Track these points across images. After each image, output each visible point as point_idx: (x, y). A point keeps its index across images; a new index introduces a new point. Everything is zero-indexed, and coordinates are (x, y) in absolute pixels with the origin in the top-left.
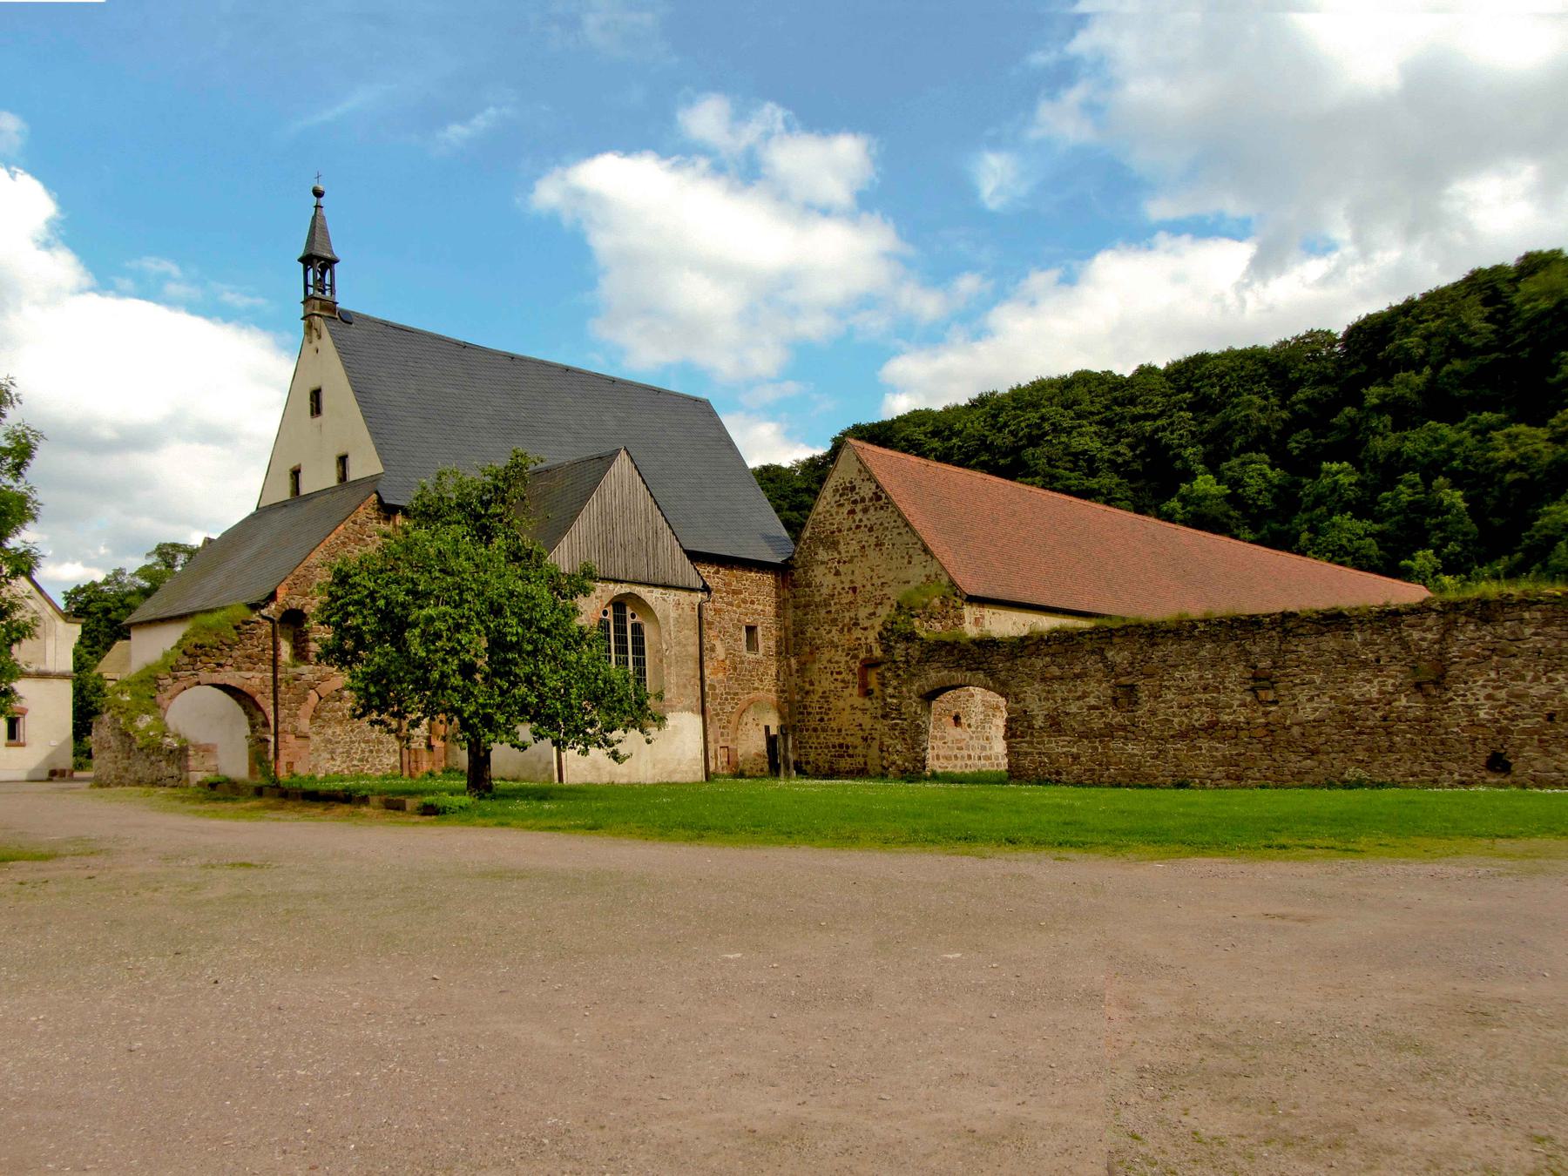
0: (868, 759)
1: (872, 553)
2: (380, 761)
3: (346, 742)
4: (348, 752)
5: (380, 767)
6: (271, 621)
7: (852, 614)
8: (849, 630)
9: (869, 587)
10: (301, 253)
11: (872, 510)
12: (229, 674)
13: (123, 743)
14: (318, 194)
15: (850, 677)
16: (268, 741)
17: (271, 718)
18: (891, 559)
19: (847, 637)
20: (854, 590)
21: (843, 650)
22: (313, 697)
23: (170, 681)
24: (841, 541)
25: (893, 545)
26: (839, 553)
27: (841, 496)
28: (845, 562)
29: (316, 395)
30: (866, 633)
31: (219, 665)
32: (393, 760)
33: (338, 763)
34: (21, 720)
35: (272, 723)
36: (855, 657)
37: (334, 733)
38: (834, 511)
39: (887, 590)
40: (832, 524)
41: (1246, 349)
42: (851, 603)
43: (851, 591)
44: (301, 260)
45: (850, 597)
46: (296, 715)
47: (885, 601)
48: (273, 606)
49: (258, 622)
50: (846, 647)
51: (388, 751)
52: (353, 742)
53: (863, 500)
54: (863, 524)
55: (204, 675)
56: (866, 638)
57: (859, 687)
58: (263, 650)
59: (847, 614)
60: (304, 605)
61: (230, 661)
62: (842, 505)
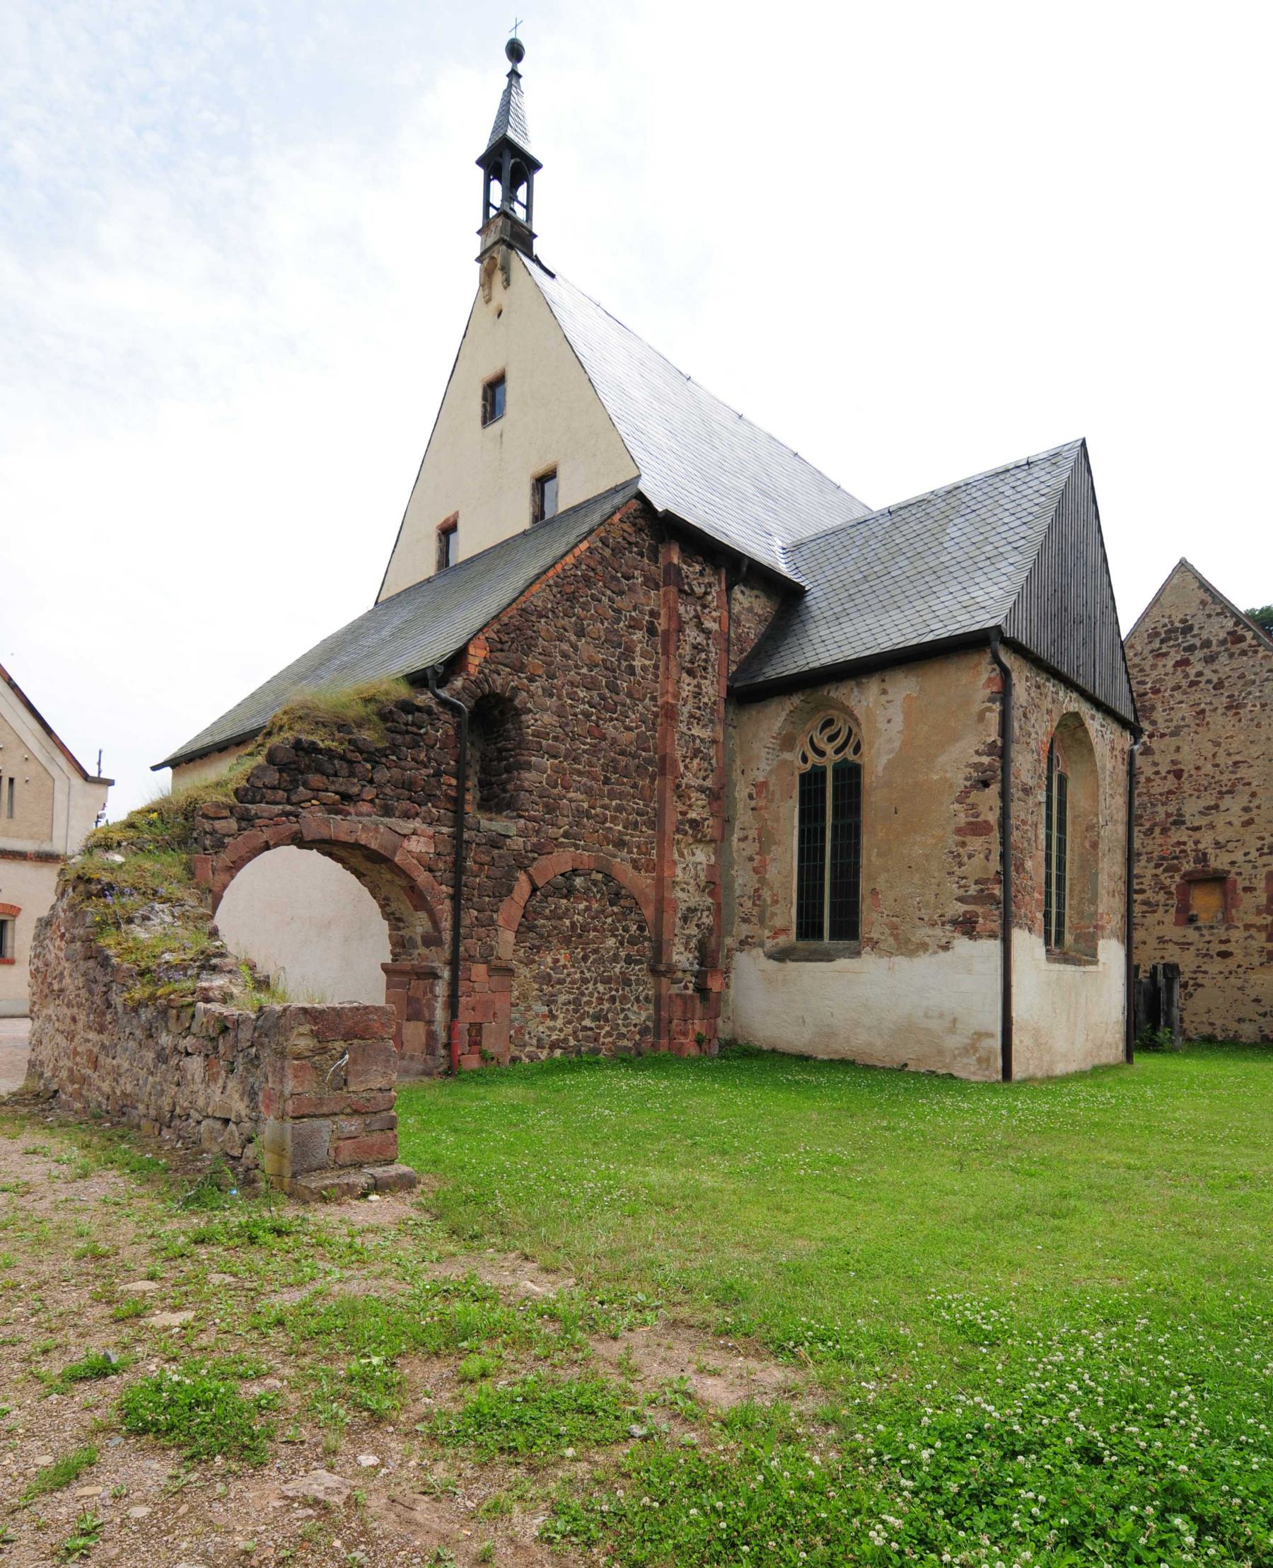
0: (1184, 1013)
1: (1220, 722)
2: (626, 1018)
3: (573, 982)
4: (576, 1002)
5: (624, 1030)
6: (454, 709)
7: (1172, 809)
8: (1164, 831)
9: (1208, 768)
10: (481, 147)
11: (1223, 658)
12: (365, 819)
13: (90, 982)
14: (515, 51)
15: (1161, 897)
16: (434, 976)
17: (446, 924)
18: (1258, 725)
19: (1160, 841)
20: (1178, 774)
21: (1149, 861)
22: (522, 887)
23: (233, 824)
24: (1159, 705)
25: (1263, 706)
26: (1154, 723)
27: (1162, 642)
28: (1163, 735)
29: (493, 391)
30: (1197, 835)
31: (346, 797)
32: (644, 1015)
33: (559, 1023)
34: (9, 925)
35: (447, 936)
36: (1172, 869)
37: (556, 961)
38: (1147, 665)
39: (1243, 772)
40: (1144, 683)
41: (1253, 610)
42: (1170, 792)
43: (1171, 777)
44: (481, 162)
45: (1171, 783)
46: (492, 923)
47: (1240, 787)
48: (458, 683)
49: (429, 711)
50: (1155, 855)
51: (637, 999)
52: (585, 981)
53: (1207, 644)
54: (1203, 679)
55: (314, 819)
56: (1197, 842)
57: (1177, 911)
58: (438, 774)
59: (1161, 809)
60: (516, 690)
61: (369, 792)
62: (1165, 655)
